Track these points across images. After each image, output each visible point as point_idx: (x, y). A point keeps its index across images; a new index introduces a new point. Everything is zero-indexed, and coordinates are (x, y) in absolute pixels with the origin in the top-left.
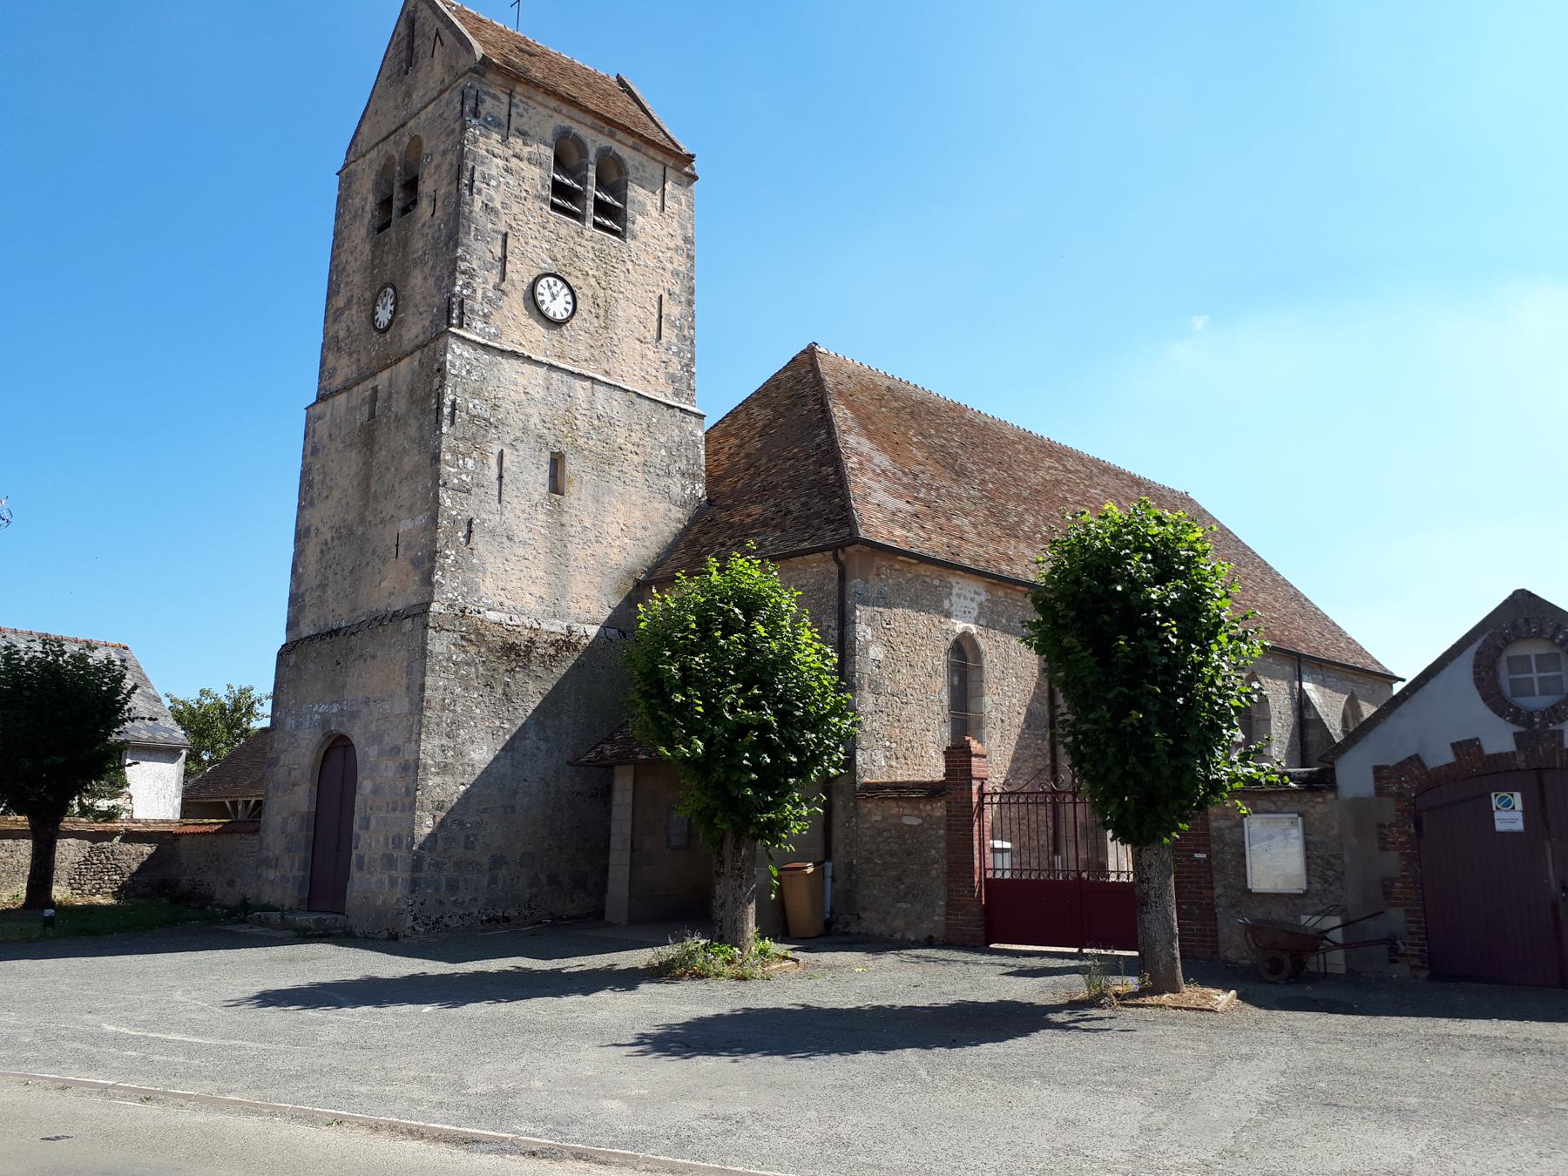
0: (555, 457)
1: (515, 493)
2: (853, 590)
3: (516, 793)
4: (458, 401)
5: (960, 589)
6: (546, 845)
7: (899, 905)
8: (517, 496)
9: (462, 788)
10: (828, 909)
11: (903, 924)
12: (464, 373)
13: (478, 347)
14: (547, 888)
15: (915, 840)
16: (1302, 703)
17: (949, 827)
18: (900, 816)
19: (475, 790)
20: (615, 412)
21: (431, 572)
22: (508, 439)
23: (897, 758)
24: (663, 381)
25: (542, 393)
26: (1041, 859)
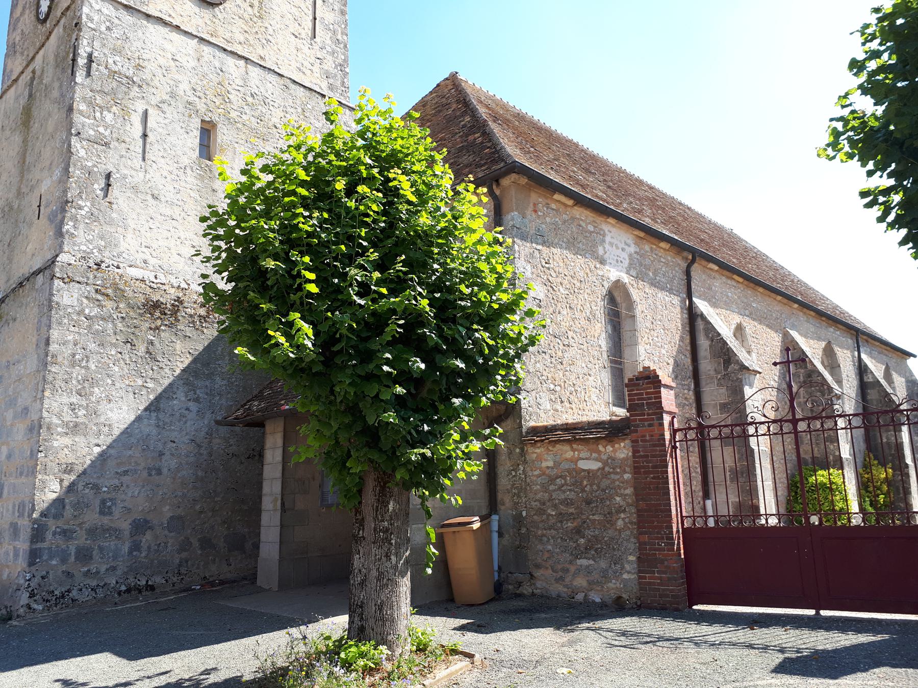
0: (207, 126)
1: (161, 154)
2: (511, 223)
3: (161, 454)
4: (96, 54)
5: (612, 237)
6: (198, 507)
7: (579, 562)
8: (163, 157)
9: (97, 450)
10: (496, 568)
11: (585, 584)
12: (103, 28)
13: (120, 7)
14: (199, 552)
15: (595, 487)
16: (862, 370)
17: (636, 470)
18: (575, 461)
19: (112, 451)
20: (270, 93)
21: (62, 223)
22: (154, 100)
23: (562, 402)
24: (318, 75)
25: (193, 63)
26: (695, 504)
